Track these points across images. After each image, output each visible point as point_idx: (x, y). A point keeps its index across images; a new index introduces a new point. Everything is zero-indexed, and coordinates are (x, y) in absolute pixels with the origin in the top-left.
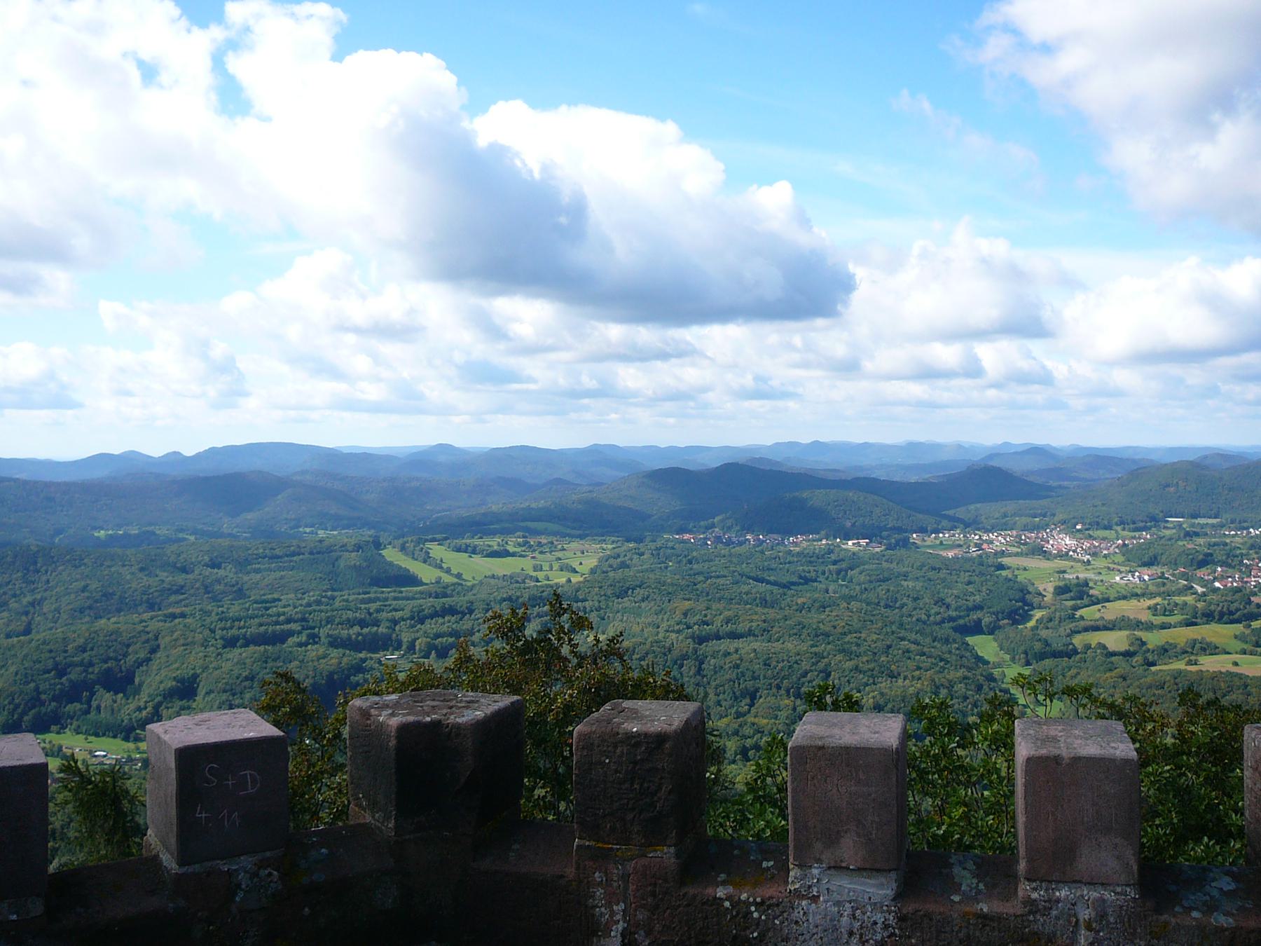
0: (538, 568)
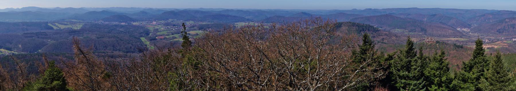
0: (73, 27)
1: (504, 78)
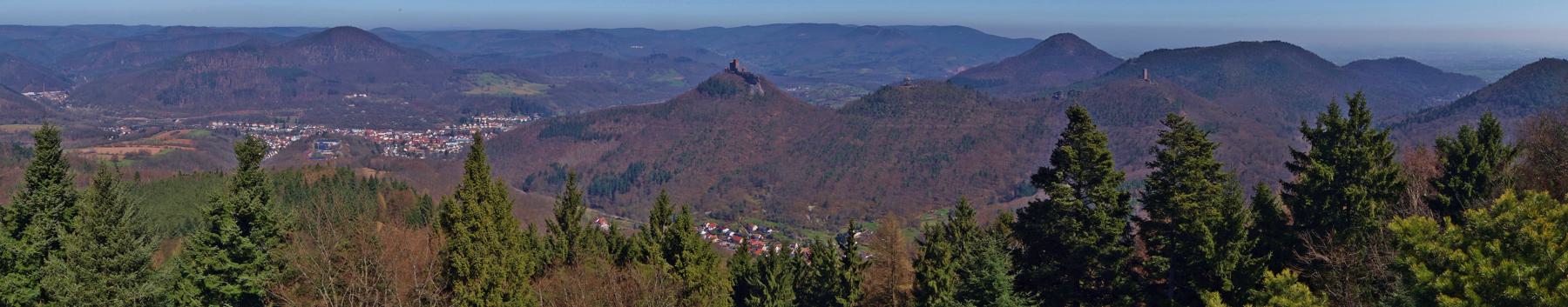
1: (120, 255)
